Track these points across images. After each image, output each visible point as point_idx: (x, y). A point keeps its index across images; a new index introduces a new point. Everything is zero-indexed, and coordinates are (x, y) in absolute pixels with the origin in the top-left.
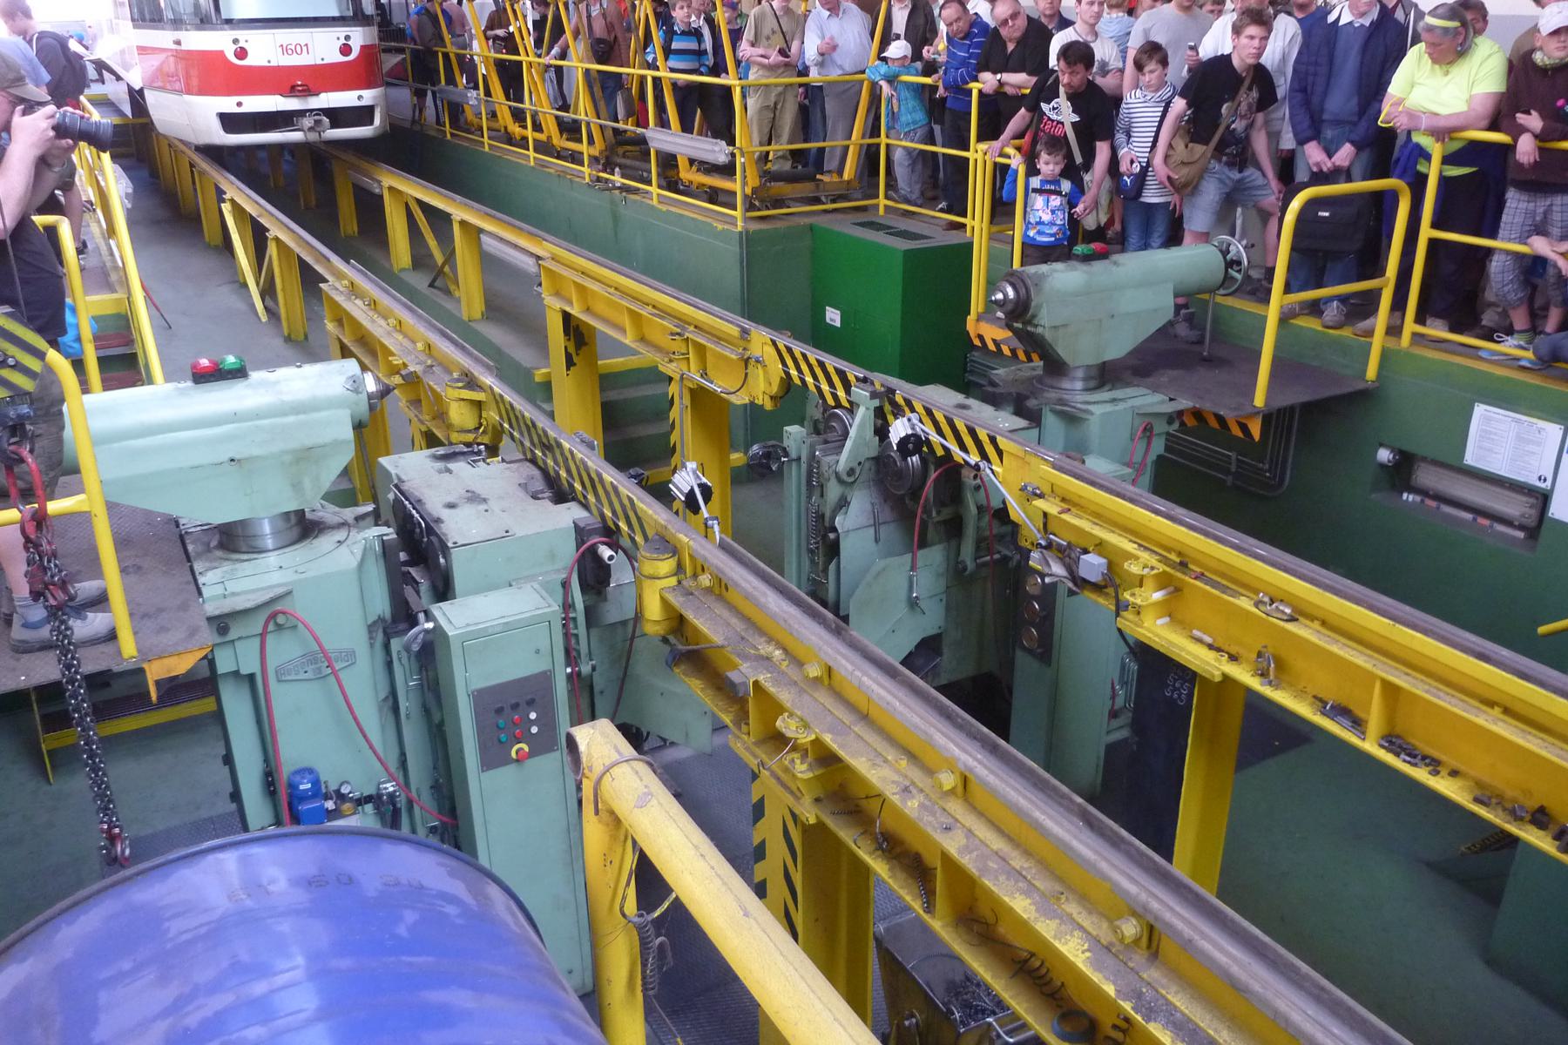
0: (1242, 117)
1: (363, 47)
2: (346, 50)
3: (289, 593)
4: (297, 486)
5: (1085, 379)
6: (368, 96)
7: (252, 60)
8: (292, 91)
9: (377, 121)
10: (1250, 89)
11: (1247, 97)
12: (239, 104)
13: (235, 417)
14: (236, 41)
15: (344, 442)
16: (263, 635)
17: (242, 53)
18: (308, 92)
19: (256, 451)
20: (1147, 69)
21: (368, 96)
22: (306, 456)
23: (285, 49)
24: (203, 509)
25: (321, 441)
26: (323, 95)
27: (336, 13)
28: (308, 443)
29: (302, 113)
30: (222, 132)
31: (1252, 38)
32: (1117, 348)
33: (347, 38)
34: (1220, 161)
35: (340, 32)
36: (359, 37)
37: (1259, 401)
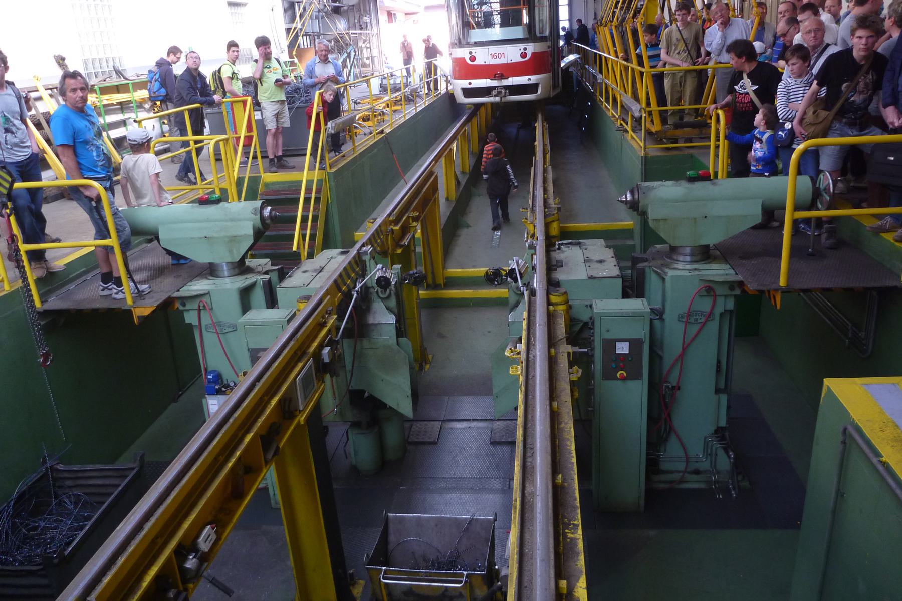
0: (861, 93)
1: (533, 54)
2: (523, 55)
3: (209, 293)
4: (230, 252)
5: (692, 255)
6: (533, 79)
7: (479, 61)
8: (494, 77)
9: (539, 92)
10: (867, 73)
11: (864, 80)
12: (470, 84)
13: (208, 220)
14: (471, 53)
15: (249, 236)
16: (199, 310)
17: (473, 59)
18: (502, 77)
19: (215, 235)
20: (790, 62)
21: (533, 79)
22: (233, 240)
23: (493, 56)
24: (201, 256)
25: (239, 234)
26: (510, 79)
27: (521, 36)
28: (235, 234)
29: (494, 88)
30: (463, 97)
31: (860, 37)
32: (712, 238)
33: (525, 49)
34: (841, 122)
35: (522, 46)
36: (531, 48)
37: (782, 282)
